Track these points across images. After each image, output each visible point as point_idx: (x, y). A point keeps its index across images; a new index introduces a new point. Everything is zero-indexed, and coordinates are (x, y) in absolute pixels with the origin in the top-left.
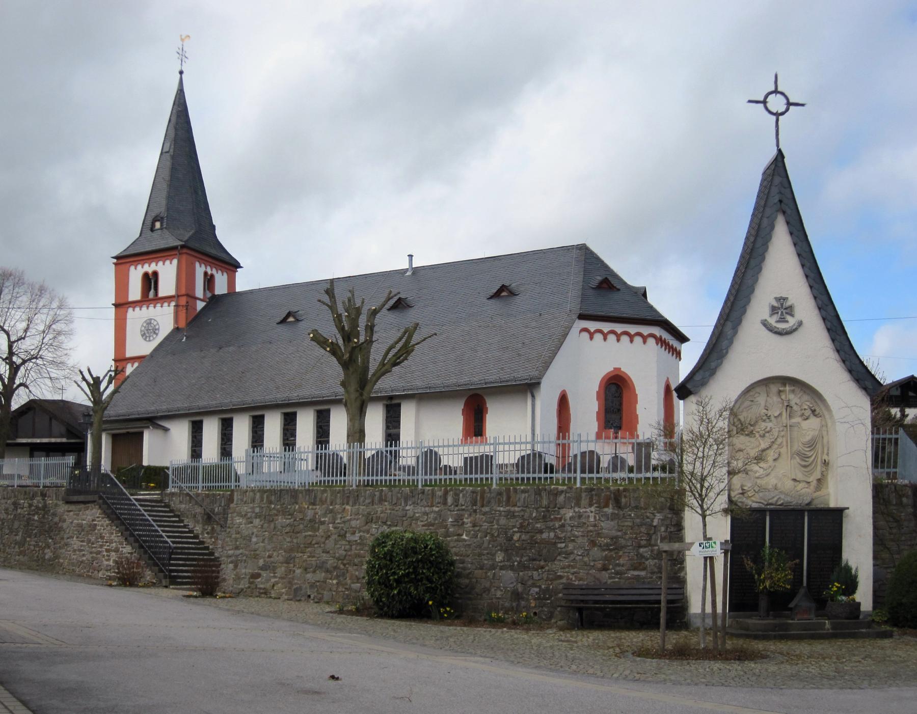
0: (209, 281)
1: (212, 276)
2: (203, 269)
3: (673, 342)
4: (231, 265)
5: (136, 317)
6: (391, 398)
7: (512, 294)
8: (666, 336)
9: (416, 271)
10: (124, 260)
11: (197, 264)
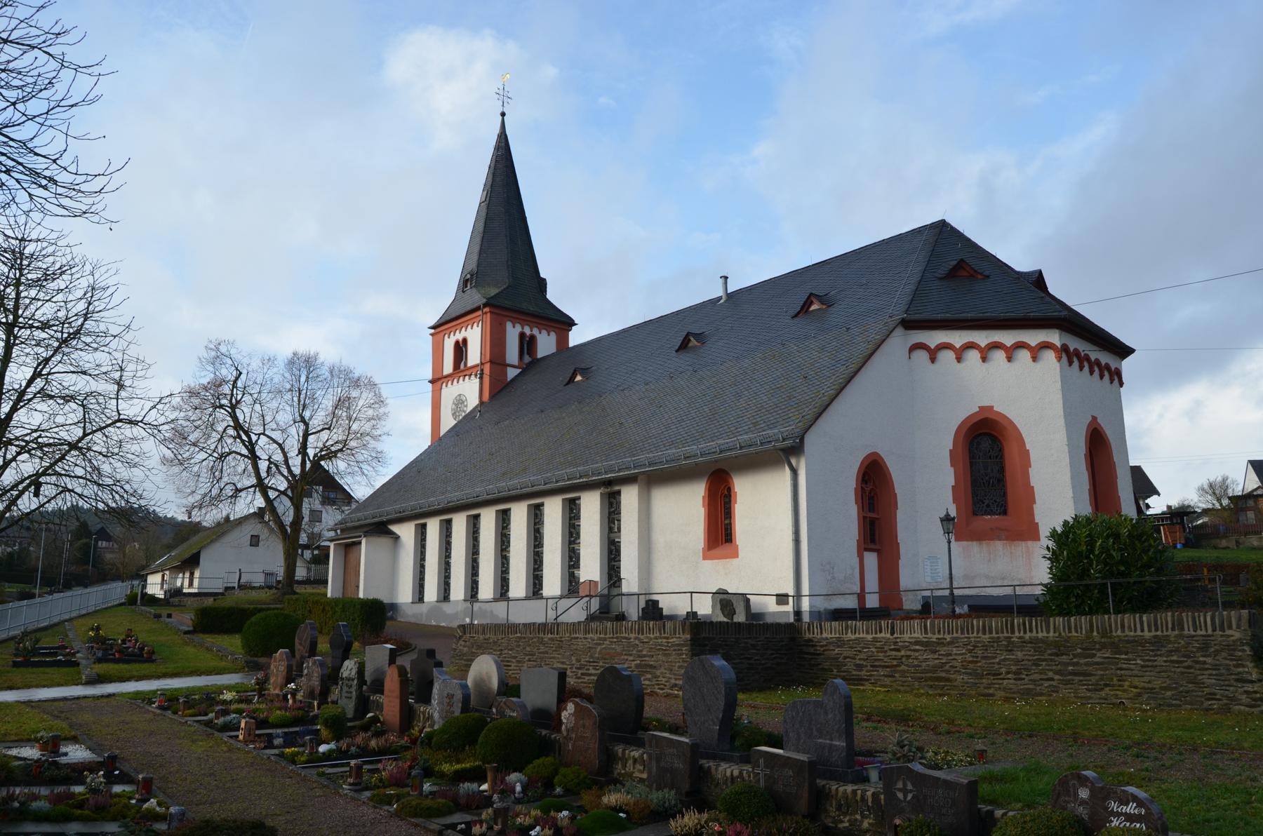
0: (527, 344)
1: (533, 338)
2: (518, 328)
3: (1105, 358)
4: (566, 323)
5: (450, 392)
6: (608, 483)
7: (827, 301)
8: (1074, 344)
9: (730, 296)
10: (442, 326)
11: (509, 325)
